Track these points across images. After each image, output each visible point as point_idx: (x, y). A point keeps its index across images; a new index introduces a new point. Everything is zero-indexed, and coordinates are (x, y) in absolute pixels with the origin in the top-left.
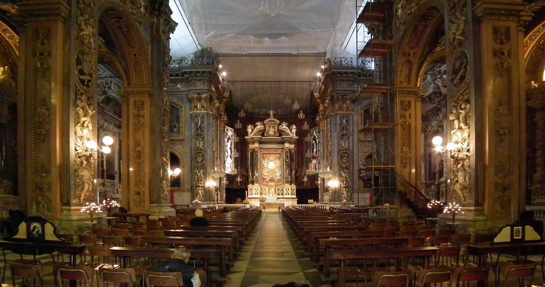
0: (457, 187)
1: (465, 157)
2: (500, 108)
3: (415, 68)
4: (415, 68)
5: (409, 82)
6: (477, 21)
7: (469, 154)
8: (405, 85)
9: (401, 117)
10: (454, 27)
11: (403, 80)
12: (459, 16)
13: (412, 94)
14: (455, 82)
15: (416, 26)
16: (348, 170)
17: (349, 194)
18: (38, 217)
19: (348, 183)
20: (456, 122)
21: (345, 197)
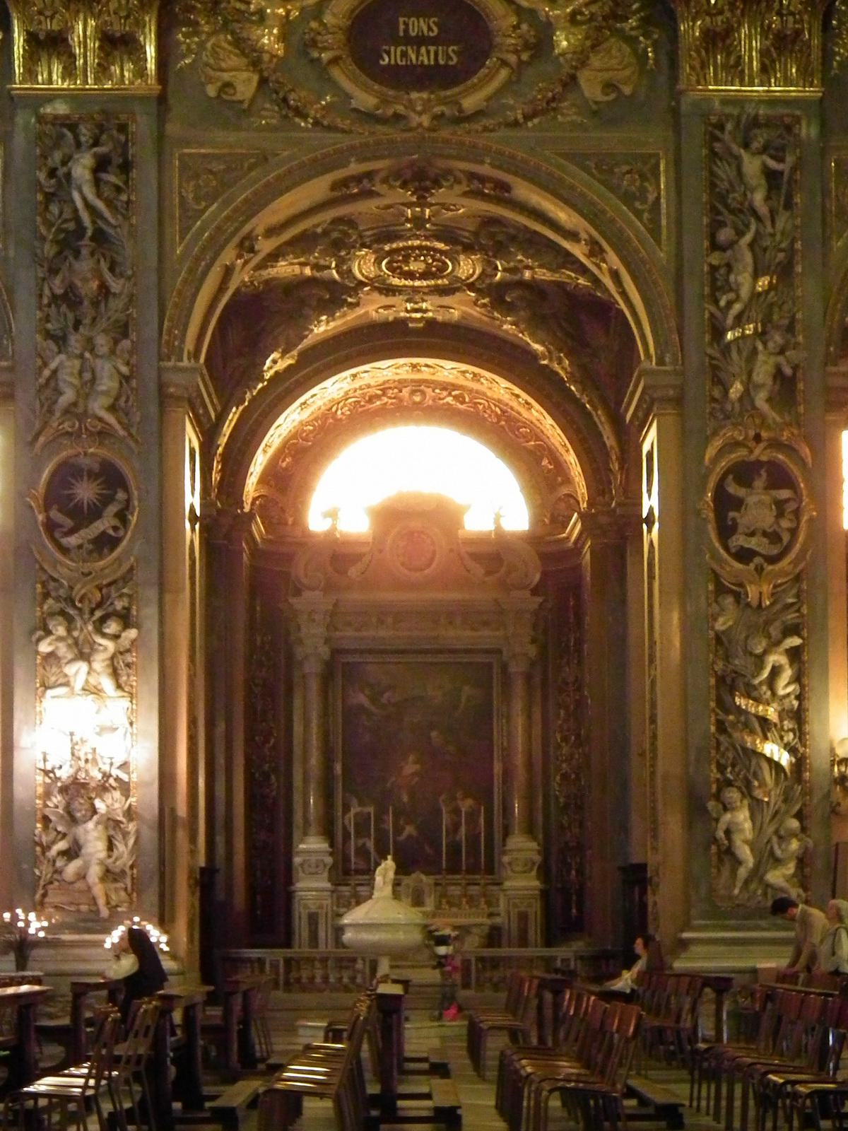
7: (125, 777)
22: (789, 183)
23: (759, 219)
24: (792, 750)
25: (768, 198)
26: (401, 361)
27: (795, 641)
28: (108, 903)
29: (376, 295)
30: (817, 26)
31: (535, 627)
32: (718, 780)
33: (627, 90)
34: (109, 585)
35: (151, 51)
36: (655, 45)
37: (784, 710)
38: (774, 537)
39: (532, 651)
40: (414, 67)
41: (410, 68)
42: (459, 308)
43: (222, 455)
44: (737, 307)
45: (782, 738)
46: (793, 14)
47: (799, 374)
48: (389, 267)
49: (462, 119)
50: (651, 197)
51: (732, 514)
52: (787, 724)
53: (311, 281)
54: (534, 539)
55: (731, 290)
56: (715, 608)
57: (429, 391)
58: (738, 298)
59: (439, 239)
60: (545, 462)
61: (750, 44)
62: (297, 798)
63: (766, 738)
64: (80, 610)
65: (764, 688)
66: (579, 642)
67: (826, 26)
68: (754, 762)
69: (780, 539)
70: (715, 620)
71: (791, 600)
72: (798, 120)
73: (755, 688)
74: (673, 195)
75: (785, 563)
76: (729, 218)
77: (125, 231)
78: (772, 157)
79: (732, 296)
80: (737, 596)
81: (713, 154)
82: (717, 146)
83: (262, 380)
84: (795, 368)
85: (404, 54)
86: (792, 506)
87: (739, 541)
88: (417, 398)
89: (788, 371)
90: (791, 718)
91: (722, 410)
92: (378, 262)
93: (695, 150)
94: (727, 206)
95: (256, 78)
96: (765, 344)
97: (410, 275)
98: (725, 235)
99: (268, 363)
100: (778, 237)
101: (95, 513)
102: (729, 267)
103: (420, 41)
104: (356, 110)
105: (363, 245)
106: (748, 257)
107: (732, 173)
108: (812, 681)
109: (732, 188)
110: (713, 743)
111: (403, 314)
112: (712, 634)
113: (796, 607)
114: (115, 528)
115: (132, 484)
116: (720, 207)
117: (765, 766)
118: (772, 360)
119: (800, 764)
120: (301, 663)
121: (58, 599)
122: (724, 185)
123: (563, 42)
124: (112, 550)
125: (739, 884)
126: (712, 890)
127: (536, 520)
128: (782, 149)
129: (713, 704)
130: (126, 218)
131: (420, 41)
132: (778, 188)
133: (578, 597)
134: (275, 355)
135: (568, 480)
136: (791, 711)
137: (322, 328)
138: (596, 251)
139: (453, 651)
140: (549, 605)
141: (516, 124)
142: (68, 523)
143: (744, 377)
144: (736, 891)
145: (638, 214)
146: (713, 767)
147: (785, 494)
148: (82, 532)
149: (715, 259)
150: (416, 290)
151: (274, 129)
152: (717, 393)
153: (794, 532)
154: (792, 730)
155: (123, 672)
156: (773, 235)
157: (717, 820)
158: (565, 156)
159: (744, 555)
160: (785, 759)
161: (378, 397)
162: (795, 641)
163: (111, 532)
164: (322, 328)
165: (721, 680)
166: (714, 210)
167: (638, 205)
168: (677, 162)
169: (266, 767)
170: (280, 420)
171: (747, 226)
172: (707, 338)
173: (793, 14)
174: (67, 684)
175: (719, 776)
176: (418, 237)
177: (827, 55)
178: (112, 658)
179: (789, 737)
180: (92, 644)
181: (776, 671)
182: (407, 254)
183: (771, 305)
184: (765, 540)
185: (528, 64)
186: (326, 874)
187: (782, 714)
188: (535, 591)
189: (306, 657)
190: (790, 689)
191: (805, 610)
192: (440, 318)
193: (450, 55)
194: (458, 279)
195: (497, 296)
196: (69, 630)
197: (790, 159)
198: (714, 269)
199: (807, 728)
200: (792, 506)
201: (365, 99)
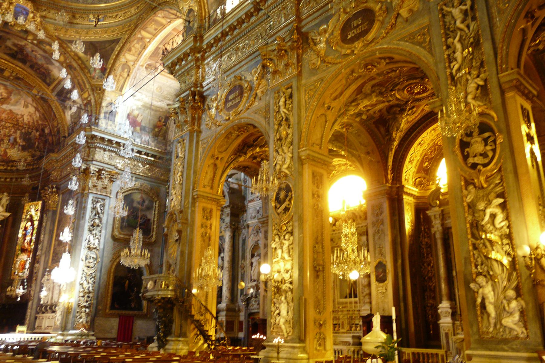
0: (282, 321)
1: (287, 289)
2: (317, 246)
3: (219, 172)
4: (219, 172)
5: (212, 188)
6: (301, 162)
7: (291, 287)
8: (208, 189)
9: (202, 226)
10: (279, 158)
11: (206, 184)
12: (286, 151)
13: (215, 201)
14: (279, 211)
15: (231, 133)
16: (93, 279)
17: (89, 319)
18: (118, 332)
19: (91, 300)
20: (279, 251)
21: (82, 322)
28: (287, 332)
37: (502, 235)
38: (484, 155)
41: (355, 36)
44: (456, 67)
51: (467, 150)
52: (505, 241)
56: (465, 192)
65: (489, 225)
68: (489, 262)
69: (488, 156)
71: (498, 182)
87: (471, 160)
90: (507, 238)
101: (284, 201)
106: (459, 46)
108: (513, 218)
112: (465, 204)
113: (501, 184)
114: (289, 205)
115: (292, 189)
117: (495, 264)
119: (513, 262)
125: (492, 325)
126: (479, 329)
129: (469, 236)
136: (506, 235)
141: (384, 37)
144: (491, 329)
145: (424, 48)
147: (487, 135)
153: (494, 151)
154: (508, 244)
155: (291, 251)
157: (478, 292)
158: (399, 40)
165: (472, 225)
172: (449, 82)
178: (289, 246)
179: (507, 248)
181: (493, 216)
184: (481, 157)
185: (386, 17)
186: (450, 316)
187: (501, 237)
189: (435, 232)
190: (503, 224)
191: (505, 185)
199: (514, 242)
200: (492, 139)
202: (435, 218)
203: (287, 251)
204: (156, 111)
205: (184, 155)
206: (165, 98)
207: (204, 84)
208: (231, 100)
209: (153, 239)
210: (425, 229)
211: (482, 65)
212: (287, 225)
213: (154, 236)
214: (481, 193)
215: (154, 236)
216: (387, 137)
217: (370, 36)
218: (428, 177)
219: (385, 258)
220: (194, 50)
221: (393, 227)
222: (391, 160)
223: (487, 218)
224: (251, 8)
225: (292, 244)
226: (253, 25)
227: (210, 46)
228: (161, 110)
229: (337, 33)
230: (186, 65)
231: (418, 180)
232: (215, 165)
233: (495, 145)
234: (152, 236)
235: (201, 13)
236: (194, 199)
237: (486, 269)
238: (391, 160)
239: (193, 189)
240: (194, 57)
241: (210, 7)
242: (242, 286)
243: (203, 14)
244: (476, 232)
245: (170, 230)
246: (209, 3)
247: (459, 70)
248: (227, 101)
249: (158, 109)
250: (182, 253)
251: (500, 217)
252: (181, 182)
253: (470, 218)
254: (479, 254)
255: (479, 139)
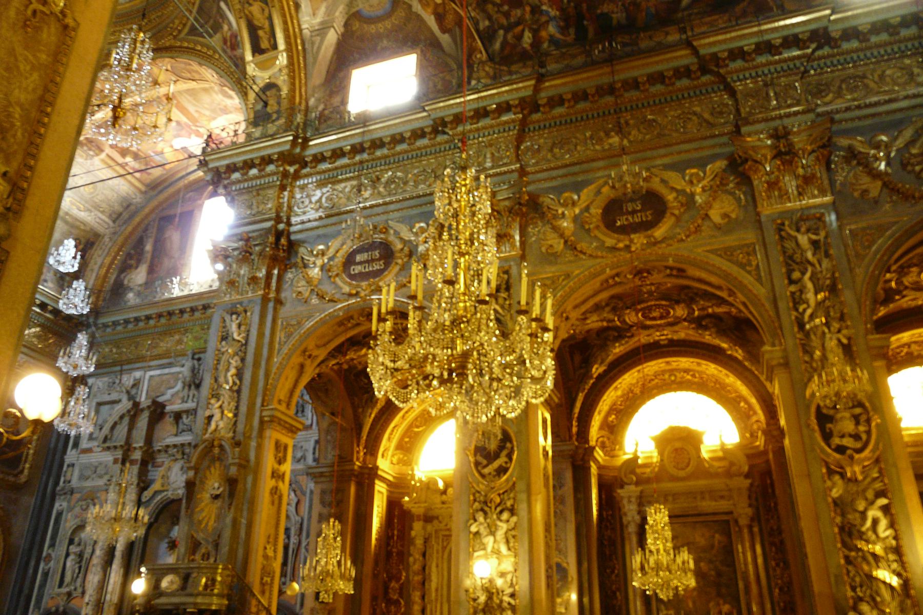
7: (512, 602)
14: (486, 471)
22: (825, 244)
23: (812, 265)
24: (899, 575)
25: (814, 255)
26: (660, 361)
27: (883, 501)
29: (641, 331)
30: (823, 169)
31: (749, 497)
32: (852, 597)
33: (733, 216)
34: (503, 493)
35: (517, 238)
36: (745, 194)
38: (856, 437)
39: (750, 511)
40: (631, 224)
41: (630, 225)
42: (683, 333)
43: (578, 418)
44: (809, 312)
45: (889, 566)
46: (810, 167)
47: (852, 342)
48: (642, 315)
49: (656, 243)
50: (754, 263)
52: (892, 557)
53: (607, 329)
54: (740, 446)
55: (804, 303)
56: (829, 483)
57: (678, 374)
58: (809, 306)
59: (663, 299)
60: (742, 404)
61: (790, 184)
62: (631, 606)
63: (878, 567)
64: (490, 508)
66: (776, 504)
67: (828, 169)
68: (874, 584)
70: (831, 490)
71: (876, 475)
72: (823, 214)
73: (863, 533)
74: (765, 260)
75: (866, 453)
76: (795, 266)
77: (508, 317)
78: (814, 234)
79: (805, 306)
80: (843, 475)
81: (782, 238)
82: (783, 233)
83: (591, 377)
84: (849, 339)
85: (627, 219)
86: (863, 418)
87: (836, 441)
88: (673, 378)
89: (845, 341)
90: (893, 553)
91: (812, 367)
92: (637, 315)
93: (772, 237)
94: (794, 261)
95: (562, 241)
96: (829, 328)
97: (654, 319)
98: (796, 275)
99: (594, 370)
100: (824, 273)
101: (497, 456)
102: (801, 291)
103: (634, 212)
104: (608, 247)
105: (627, 308)
106: (810, 285)
107: (793, 245)
108: (902, 527)
109: (795, 253)
110: (845, 571)
111: (657, 338)
112: (830, 500)
114: (506, 463)
115: (514, 439)
116: (790, 262)
117: (882, 586)
118: (834, 337)
119: (906, 584)
120: (627, 526)
121: (479, 502)
122: (791, 251)
123: (699, 199)
124: (505, 474)
127: (742, 436)
128: (817, 229)
129: (839, 545)
130: (509, 311)
131: (634, 212)
132: (819, 248)
133: (771, 478)
134: (596, 366)
135: (755, 413)
137: (618, 350)
138: (731, 293)
139: (707, 514)
140: (756, 484)
141: (682, 240)
142: (485, 462)
143: (820, 348)
145: (749, 272)
146: (848, 588)
148: (490, 467)
149: (793, 288)
150: (659, 326)
151: (570, 262)
152: (807, 358)
153: (869, 433)
155: (512, 541)
156: (821, 272)
159: (841, 450)
160: (895, 581)
161: (653, 380)
162: (883, 501)
163: (504, 465)
164: (618, 350)
165: (842, 529)
166: (787, 265)
167: (748, 268)
168: (765, 245)
169: (614, 587)
170: (605, 397)
171: (806, 270)
172: (796, 329)
173: (810, 167)
174: (484, 549)
175: (852, 594)
176: (652, 300)
177: (832, 183)
178: (506, 533)
179: (895, 566)
180: (496, 525)
181: (875, 522)
182: (650, 309)
183: (828, 307)
185: (684, 213)
187: (887, 549)
188: (747, 476)
189: (629, 522)
192: (675, 338)
193: (648, 216)
194: (678, 318)
195: (698, 323)
196: (485, 519)
197: (823, 234)
198: (793, 293)
199: (905, 559)
201: (610, 242)
202: (630, 502)
203: (504, 540)
204: (73, 226)
205: (247, 339)
206: (97, 207)
207: (294, 220)
208: (360, 263)
209: (23, 478)
210: (607, 515)
211: (842, 318)
212: (506, 496)
213: (26, 472)
214: (853, 488)
215: (26, 472)
216: (582, 371)
217: (659, 232)
218: (612, 437)
219: (566, 557)
220: (286, 158)
221: (577, 511)
222: (578, 405)
223: (869, 523)
224: (427, 127)
225: (513, 529)
226: (419, 152)
227: (319, 158)
228: (82, 227)
229: (596, 211)
230: (256, 178)
231: (601, 439)
232: (302, 366)
233: (870, 426)
234: (22, 472)
235: (294, 97)
236: (262, 422)
237: (868, 592)
238: (578, 405)
239: (263, 405)
240: (281, 169)
241: (310, 92)
242: (294, 590)
243: (297, 99)
244: (847, 539)
245: (199, 475)
246: (310, 85)
247: (812, 317)
248: (349, 261)
249: (78, 223)
250: (235, 523)
251: (883, 523)
252: (235, 388)
253: (838, 520)
254: (857, 572)
255: (847, 415)
